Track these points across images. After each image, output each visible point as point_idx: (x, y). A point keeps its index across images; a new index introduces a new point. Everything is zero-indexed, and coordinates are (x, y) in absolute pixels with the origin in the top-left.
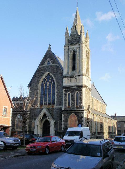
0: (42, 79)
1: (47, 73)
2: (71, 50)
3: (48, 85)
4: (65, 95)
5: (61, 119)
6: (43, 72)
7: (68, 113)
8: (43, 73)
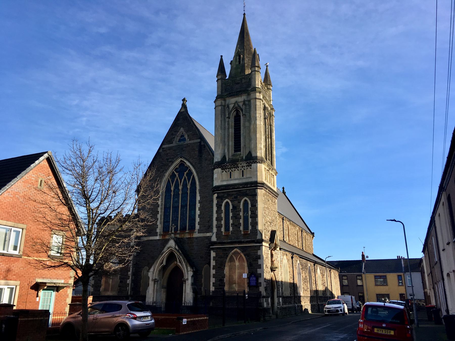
2: (231, 106)
3: (180, 188)
4: (219, 206)
7: (225, 249)
8: (170, 160)
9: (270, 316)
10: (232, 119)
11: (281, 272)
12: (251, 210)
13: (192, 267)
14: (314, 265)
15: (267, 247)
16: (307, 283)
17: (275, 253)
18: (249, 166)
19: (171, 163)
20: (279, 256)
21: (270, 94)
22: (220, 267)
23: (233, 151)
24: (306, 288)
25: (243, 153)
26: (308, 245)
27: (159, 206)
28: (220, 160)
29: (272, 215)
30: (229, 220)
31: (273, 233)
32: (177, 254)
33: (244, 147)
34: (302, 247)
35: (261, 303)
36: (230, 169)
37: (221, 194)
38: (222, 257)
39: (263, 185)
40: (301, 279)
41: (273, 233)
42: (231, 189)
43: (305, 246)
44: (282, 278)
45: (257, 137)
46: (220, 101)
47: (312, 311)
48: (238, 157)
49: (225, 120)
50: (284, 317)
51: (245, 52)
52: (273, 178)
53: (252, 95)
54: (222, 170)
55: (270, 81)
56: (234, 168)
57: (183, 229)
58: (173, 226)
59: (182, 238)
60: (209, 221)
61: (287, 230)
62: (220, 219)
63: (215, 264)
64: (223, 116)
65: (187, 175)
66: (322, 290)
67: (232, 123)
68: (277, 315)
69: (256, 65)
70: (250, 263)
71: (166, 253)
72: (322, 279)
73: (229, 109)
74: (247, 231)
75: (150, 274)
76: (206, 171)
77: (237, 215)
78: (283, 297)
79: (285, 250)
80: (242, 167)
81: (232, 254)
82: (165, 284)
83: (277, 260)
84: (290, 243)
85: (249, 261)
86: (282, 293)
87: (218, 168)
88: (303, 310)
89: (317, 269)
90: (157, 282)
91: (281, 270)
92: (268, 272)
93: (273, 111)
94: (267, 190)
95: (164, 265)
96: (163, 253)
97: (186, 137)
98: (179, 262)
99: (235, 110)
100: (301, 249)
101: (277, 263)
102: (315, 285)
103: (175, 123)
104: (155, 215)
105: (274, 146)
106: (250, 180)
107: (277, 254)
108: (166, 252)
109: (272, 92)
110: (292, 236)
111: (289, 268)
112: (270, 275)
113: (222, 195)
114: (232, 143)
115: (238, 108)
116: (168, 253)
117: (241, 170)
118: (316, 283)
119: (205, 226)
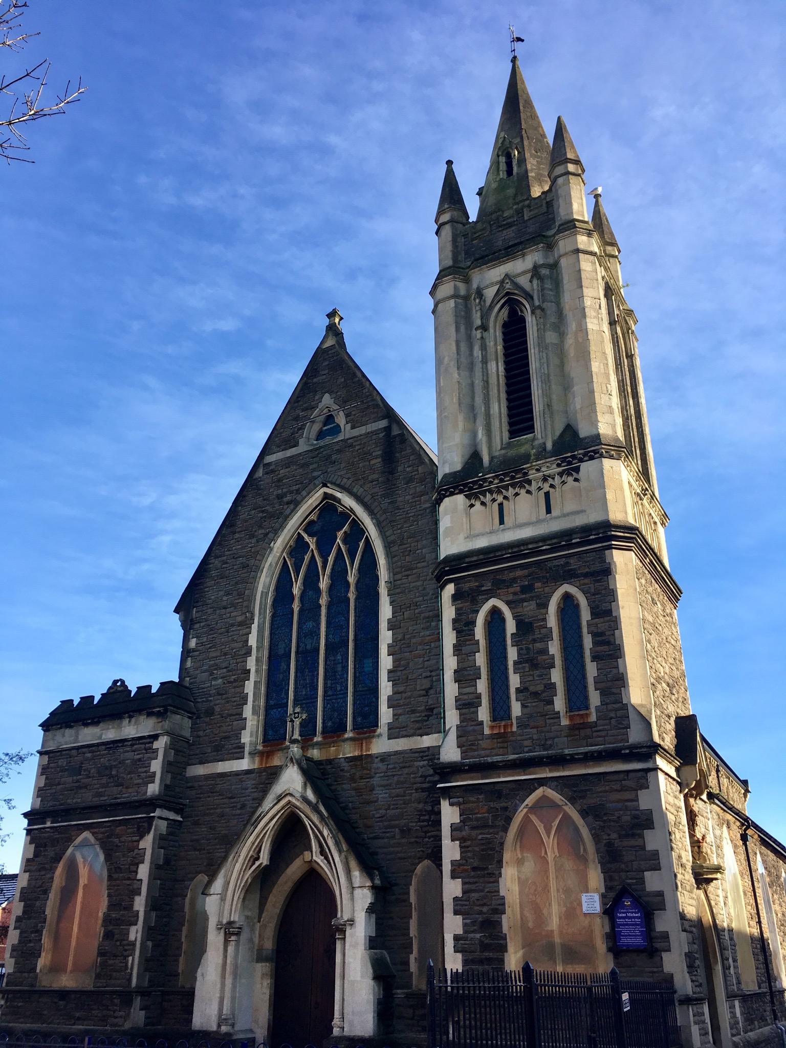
1: (314, 499)
2: (490, 293)
3: (324, 584)
4: (464, 626)
5: (436, 856)
6: (284, 495)
7: (495, 792)
8: (288, 498)
10: (495, 331)
12: (592, 628)
13: (368, 868)
18: (569, 474)
19: (292, 506)
23: (506, 435)
27: (249, 653)
28: (458, 467)
32: (310, 820)
33: (546, 410)
36: (499, 492)
46: (452, 284)
49: (469, 338)
51: (526, 143)
53: (563, 245)
54: (470, 499)
55: (612, 234)
56: (515, 488)
57: (335, 730)
58: (298, 713)
59: (330, 762)
62: (471, 673)
63: (458, 858)
64: (462, 328)
65: (345, 541)
67: (496, 344)
70: (609, 844)
73: (482, 303)
74: (581, 712)
75: (211, 904)
76: (411, 519)
80: (545, 479)
81: (526, 810)
82: (269, 945)
85: (605, 837)
87: (452, 494)
90: (238, 934)
94: (646, 559)
95: (261, 864)
96: (258, 817)
97: (341, 419)
98: (319, 850)
99: (503, 301)
103: (306, 384)
104: (234, 684)
106: (579, 521)
109: (621, 269)
114: (499, 408)
119: (413, 712)
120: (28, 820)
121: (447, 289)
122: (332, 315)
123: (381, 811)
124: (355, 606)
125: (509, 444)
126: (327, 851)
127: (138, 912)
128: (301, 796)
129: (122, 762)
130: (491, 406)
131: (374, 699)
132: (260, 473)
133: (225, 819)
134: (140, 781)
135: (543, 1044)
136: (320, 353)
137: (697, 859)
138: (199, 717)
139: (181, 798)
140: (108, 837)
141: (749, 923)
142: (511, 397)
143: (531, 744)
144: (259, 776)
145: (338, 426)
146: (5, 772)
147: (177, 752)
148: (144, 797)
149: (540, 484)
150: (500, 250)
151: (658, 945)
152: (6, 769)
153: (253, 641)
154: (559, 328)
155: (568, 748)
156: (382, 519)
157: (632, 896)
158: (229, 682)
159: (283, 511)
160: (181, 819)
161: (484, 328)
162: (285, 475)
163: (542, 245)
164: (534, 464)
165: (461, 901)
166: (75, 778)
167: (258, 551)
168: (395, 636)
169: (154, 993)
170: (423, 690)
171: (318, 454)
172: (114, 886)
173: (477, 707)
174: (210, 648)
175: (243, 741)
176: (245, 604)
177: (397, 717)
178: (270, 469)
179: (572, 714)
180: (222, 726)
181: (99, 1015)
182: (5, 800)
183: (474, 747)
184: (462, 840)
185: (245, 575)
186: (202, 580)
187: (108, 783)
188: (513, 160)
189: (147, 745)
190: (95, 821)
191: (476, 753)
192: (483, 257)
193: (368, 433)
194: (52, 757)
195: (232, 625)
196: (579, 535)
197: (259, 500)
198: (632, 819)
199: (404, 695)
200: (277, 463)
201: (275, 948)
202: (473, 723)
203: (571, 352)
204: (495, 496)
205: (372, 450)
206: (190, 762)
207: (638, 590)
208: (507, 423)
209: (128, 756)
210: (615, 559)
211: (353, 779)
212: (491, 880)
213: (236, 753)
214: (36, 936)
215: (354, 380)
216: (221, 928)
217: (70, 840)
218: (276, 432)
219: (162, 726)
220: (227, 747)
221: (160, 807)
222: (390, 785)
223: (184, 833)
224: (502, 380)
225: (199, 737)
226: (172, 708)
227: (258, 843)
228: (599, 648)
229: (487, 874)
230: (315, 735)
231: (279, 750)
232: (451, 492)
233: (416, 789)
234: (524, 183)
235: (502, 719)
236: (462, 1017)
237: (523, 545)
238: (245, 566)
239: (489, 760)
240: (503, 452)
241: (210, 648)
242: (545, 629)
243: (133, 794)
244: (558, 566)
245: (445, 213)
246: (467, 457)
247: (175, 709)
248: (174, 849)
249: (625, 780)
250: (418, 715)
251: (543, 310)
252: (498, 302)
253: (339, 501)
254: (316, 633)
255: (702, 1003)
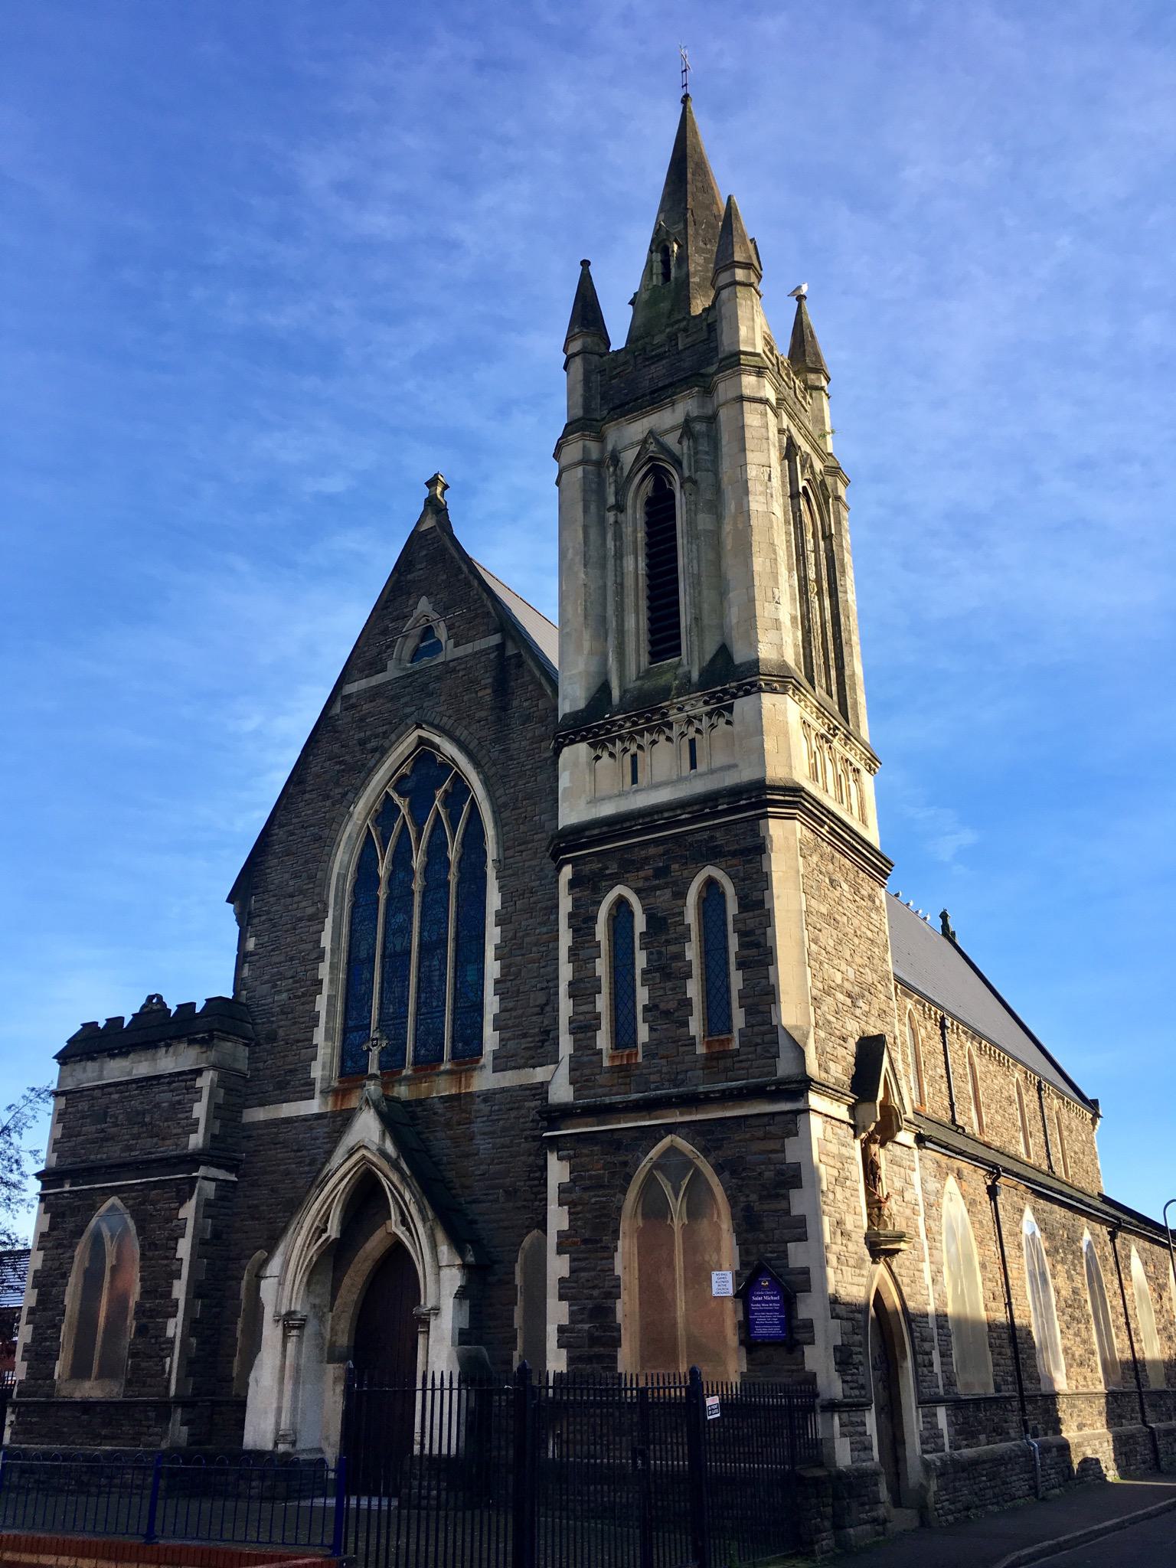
0: (361, 808)
1: (405, 746)
2: (629, 457)
3: (417, 862)
4: (582, 923)
7: (613, 1142)
8: (373, 744)
9: (875, 1521)
10: (635, 512)
11: (931, 1262)
12: (740, 926)
13: (458, 1243)
14: (1113, 1236)
15: (838, 1123)
16: (1082, 1326)
17: (889, 1157)
18: (720, 715)
19: (377, 755)
20: (916, 1177)
21: (822, 410)
22: (597, 1242)
23: (645, 659)
24: (1079, 1351)
25: (692, 658)
26: (1076, 1153)
27: (321, 957)
28: (581, 704)
29: (858, 960)
30: (634, 991)
31: (870, 1051)
32: (390, 1180)
33: (694, 626)
34: (1046, 1162)
35: (817, 1444)
36: (632, 739)
37: (591, 862)
38: (602, 1187)
39: (794, 798)
40: (1048, 1306)
41: (870, 1051)
42: (639, 833)
43: (1060, 1156)
44: (941, 1297)
45: (754, 569)
46: (581, 443)
47: (1123, 1471)
48: (669, 676)
49: (602, 521)
50: (968, 1516)
51: (691, 231)
52: (855, 781)
53: (724, 390)
54: (595, 749)
55: (817, 355)
56: (651, 734)
57: (428, 1063)
58: (377, 1039)
59: (420, 1102)
60: (542, 1009)
61: (969, 1077)
62: (589, 985)
63: (566, 1227)
64: (593, 508)
65: (445, 804)
66: (1164, 1362)
67: (635, 531)
68: (922, 1509)
69: (739, 256)
70: (748, 1208)
71: (342, 1180)
72: (1158, 1307)
73: (618, 472)
74: (722, 1037)
75: (268, 1290)
76: (528, 773)
77: (671, 958)
78: (957, 1405)
79: (942, 1147)
80: (689, 722)
81: (649, 1165)
82: (343, 1340)
83: (908, 1196)
84: (986, 1139)
85: (743, 1199)
86: (950, 1383)
87: (573, 742)
88: (1076, 1466)
89: (1128, 1257)
90: (301, 1327)
91: (931, 1255)
92: (852, 1262)
93: (840, 484)
94: (822, 827)
95: (329, 1237)
96: (325, 1177)
97: (442, 633)
98: (399, 1219)
99: (645, 469)
100: (1045, 1167)
101: (908, 1212)
102: (1124, 1336)
103: (398, 582)
104: (303, 1000)
105: (855, 639)
106: (730, 780)
107: (906, 1163)
108: (340, 1173)
109: (830, 406)
110: (993, 1106)
111: (981, 1242)
112: (864, 1281)
113: (596, 866)
114: (636, 622)
115: (660, 459)
116: (349, 1176)
117: (686, 740)
118: (1128, 1324)
119: (525, 1036)
120: (43, 1182)
121: (573, 452)
122: (432, 483)
123: (482, 1167)
124: (457, 893)
125: (648, 671)
126: (410, 1220)
127: (177, 1300)
128: (378, 1150)
129: (158, 1105)
130: (626, 618)
131: (479, 1019)
132: (337, 709)
133: (290, 1179)
134: (179, 1131)
135: (652, 1462)
136: (416, 540)
137: (876, 1224)
138: (258, 1044)
139: (234, 1151)
140: (141, 1204)
141: (986, 1305)
142: (656, 603)
143: (659, 1079)
144: (333, 1122)
145: (439, 641)
146: (31, 1113)
147: (229, 1091)
148: (185, 1151)
149: (684, 729)
150: (644, 395)
151: (798, 1337)
152: (32, 1109)
153: (326, 941)
154: (716, 507)
155: (703, 1084)
156: (490, 774)
157: (770, 1274)
158: (296, 997)
159: (366, 762)
160: (236, 1179)
161: (620, 508)
162: (370, 713)
163: (697, 389)
164: (675, 701)
165: (567, 1282)
166: (99, 1127)
167: (334, 818)
168: (504, 934)
169: (200, 1404)
170: (538, 1006)
171: (411, 682)
172: (148, 1267)
173: (595, 1031)
174: (273, 950)
175: (313, 1075)
176: (317, 890)
177: (504, 1043)
178: (350, 706)
179: (710, 1039)
180: (286, 1056)
181: (131, 1432)
182: (31, 1152)
183: (590, 1084)
184: (572, 1204)
185: (318, 851)
186: (263, 858)
187: (139, 1133)
188: (671, 258)
189: (188, 1083)
190: (124, 1183)
191: (592, 1091)
192: (622, 405)
193: (476, 653)
194: (70, 1099)
195: (300, 920)
196: (726, 800)
197: (336, 748)
198: (775, 1175)
199: (514, 1014)
200: (359, 694)
201: (352, 1344)
202: (591, 1052)
203: (729, 543)
204: (627, 744)
205: (480, 678)
206: (247, 1103)
207: (802, 870)
208: (646, 642)
209: (165, 1097)
210: (771, 832)
211: (448, 1125)
212: (606, 1255)
213: (305, 1091)
214: (53, 1333)
215: (460, 578)
216: (278, 1321)
217: (93, 1208)
218: (358, 651)
219: (207, 1057)
220: (292, 1083)
221: (205, 1164)
222: (493, 1133)
223: (239, 1197)
224: (643, 582)
225: (258, 1070)
226: (220, 1033)
227: (325, 1213)
228: (746, 952)
229: (601, 1247)
230: (404, 1066)
231: (357, 1088)
232: (571, 739)
233: (526, 1138)
234: (684, 293)
235: (626, 1047)
236: (565, 1429)
237: (657, 812)
238: (318, 838)
239: (607, 1100)
240: (639, 683)
241: (273, 950)
242: (681, 927)
243: (171, 1148)
244: (701, 841)
245: (575, 339)
246: (594, 690)
247: (225, 1035)
248: (227, 1218)
249: (769, 1125)
250: (530, 1039)
251: (695, 482)
252: (640, 470)
253: (437, 748)
254: (406, 931)
255: (864, 1410)
